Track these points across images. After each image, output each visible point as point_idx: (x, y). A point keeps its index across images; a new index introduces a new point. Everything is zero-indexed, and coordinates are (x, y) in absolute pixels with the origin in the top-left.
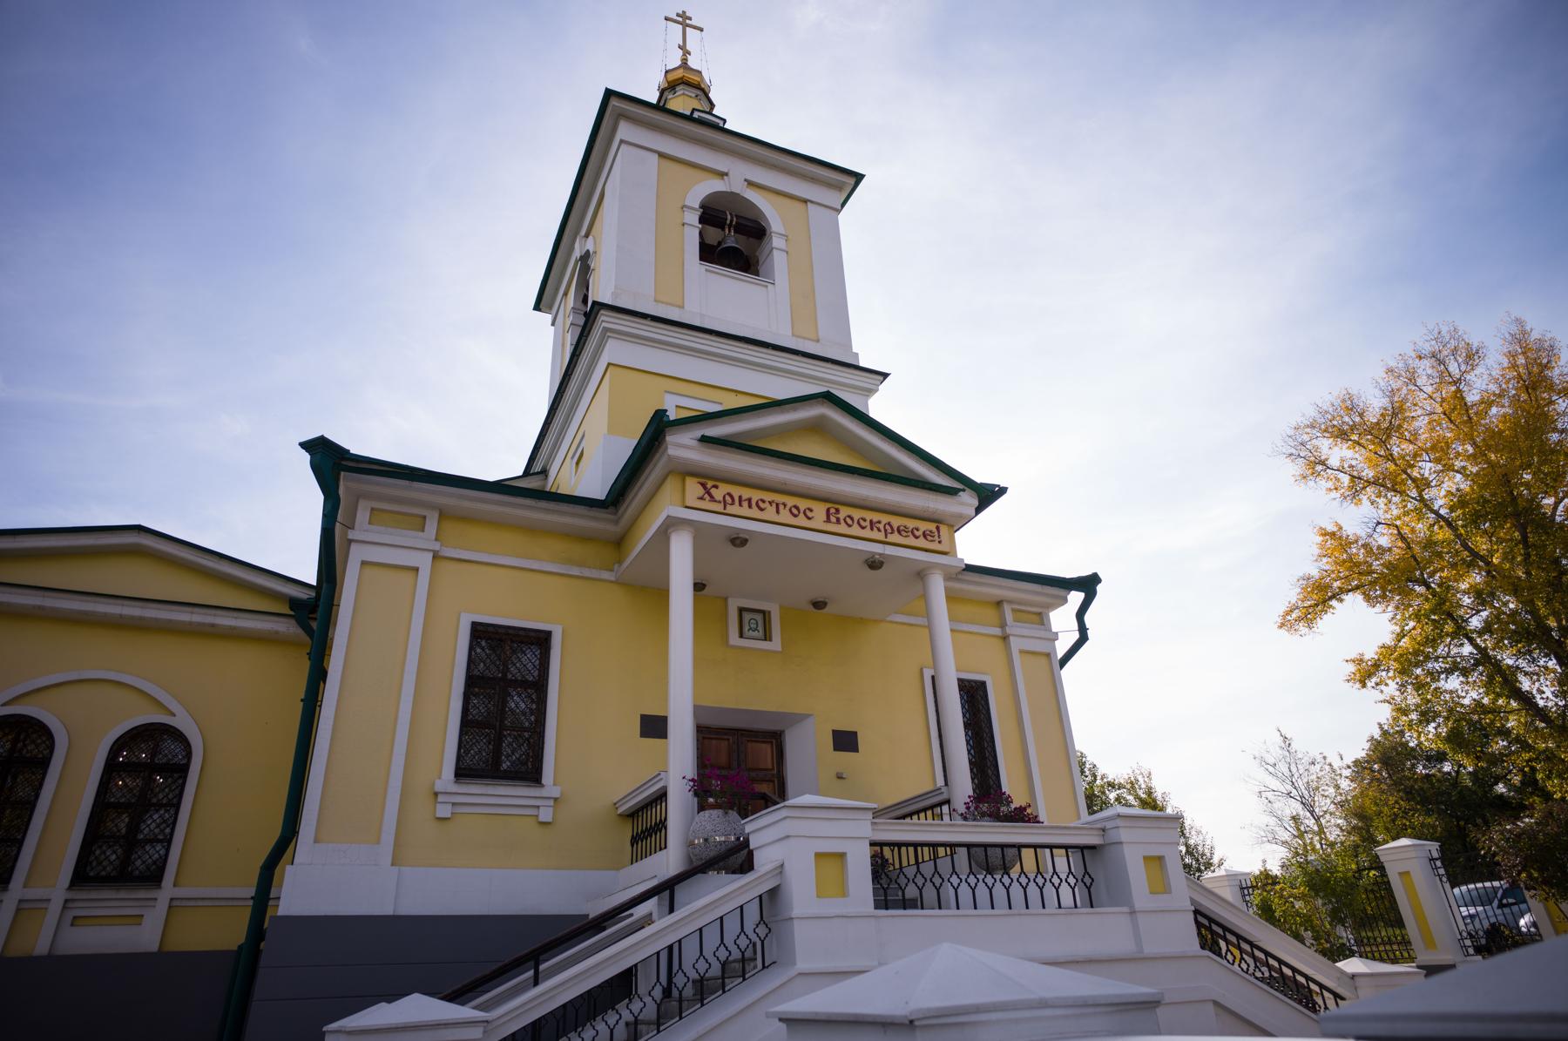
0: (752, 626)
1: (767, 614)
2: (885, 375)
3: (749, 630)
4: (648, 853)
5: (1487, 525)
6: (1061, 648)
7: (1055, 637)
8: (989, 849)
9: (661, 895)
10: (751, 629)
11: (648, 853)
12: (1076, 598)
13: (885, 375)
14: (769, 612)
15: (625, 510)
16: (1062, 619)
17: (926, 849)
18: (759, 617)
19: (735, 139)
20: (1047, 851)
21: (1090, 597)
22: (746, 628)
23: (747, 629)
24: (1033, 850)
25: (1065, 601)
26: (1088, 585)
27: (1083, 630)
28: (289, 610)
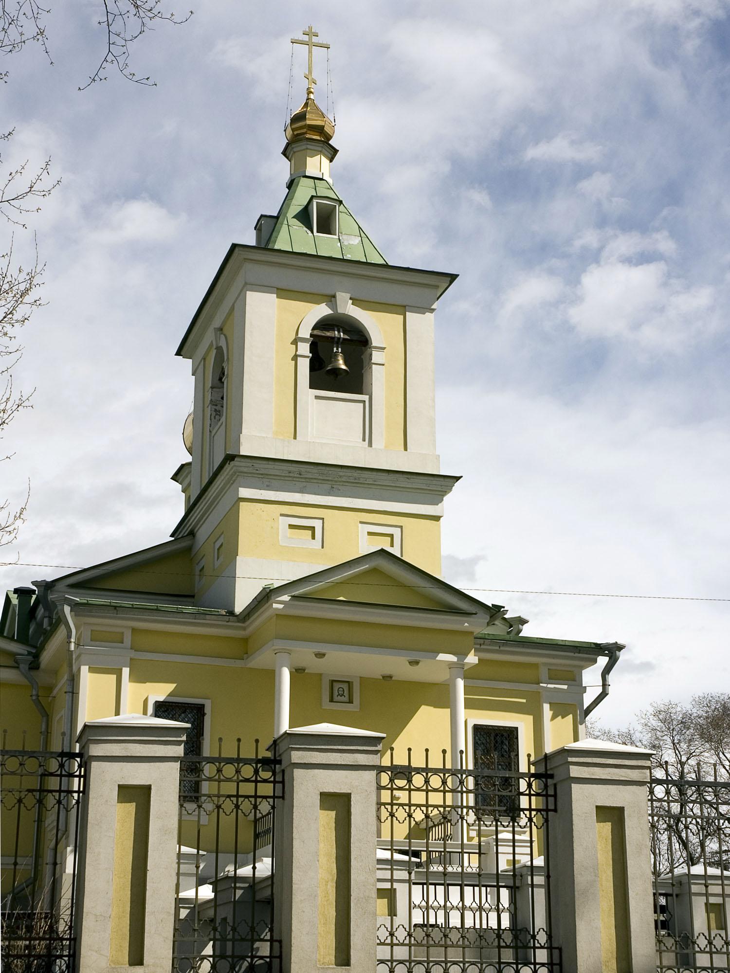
0: (340, 692)
1: (351, 683)
2: (453, 277)
3: (337, 696)
4: (266, 844)
5: (709, 721)
6: (588, 699)
7: (584, 689)
8: (451, 854)
9: (495, 832)
10: (339, 695)
11: (266, 844)
12: (603, 661)
13: (453, 277)
14: (352, 682)
15: (256, 619)
16: (591, 676)
17: (437, 853)
18: (345, 686)
19: (359, 607)
20: (467, 855)
21: (613, 661)
22: (336, 693)
23: (336, 696)
24: (468, 854)
25: (595, 661)
26: (612, 651)
27: (605, 685)
28: (13, 663)
